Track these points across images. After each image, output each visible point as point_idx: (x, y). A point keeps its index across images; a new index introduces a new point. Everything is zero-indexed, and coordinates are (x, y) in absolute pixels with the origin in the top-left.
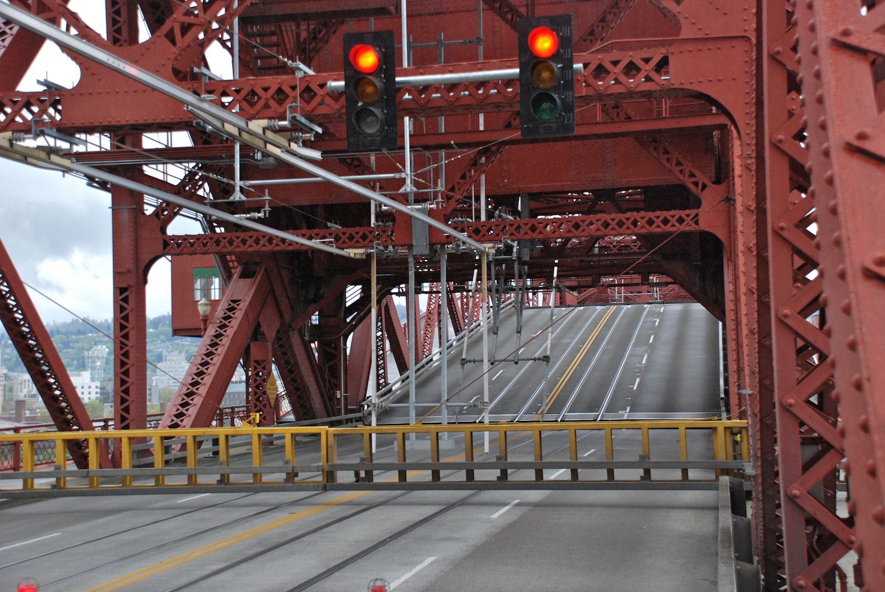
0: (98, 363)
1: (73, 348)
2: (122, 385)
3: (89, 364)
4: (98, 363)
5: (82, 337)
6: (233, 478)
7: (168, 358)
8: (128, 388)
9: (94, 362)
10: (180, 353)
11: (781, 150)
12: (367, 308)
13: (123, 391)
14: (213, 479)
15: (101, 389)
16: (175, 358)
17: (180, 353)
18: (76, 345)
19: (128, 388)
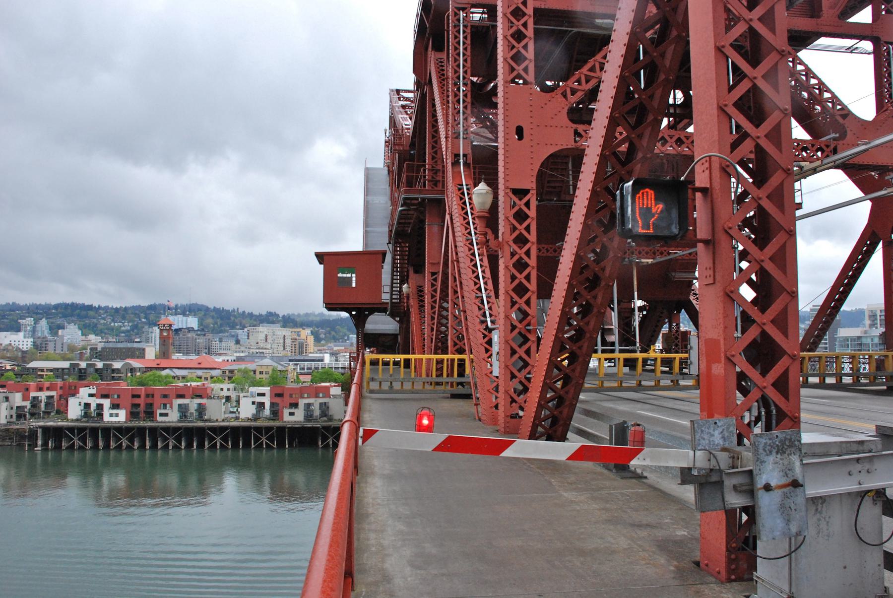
0: (29, 328)
1: (7, 319)
2: (433, 128)
3: (23, 328)
4: (29, 328)
5: (12, 313)
6: (643, 383)
7: (68, 327)
8: (437, 151)
9: (26, 327)
10: (75, 325)
11: (723, 52)
12: (687, 67)
13: (434, 142)
14: (633, 383)
15: (33, 342)
16: (72, 327)
17: (75, 325)
18: (9, 317)
19: (437, 151)
